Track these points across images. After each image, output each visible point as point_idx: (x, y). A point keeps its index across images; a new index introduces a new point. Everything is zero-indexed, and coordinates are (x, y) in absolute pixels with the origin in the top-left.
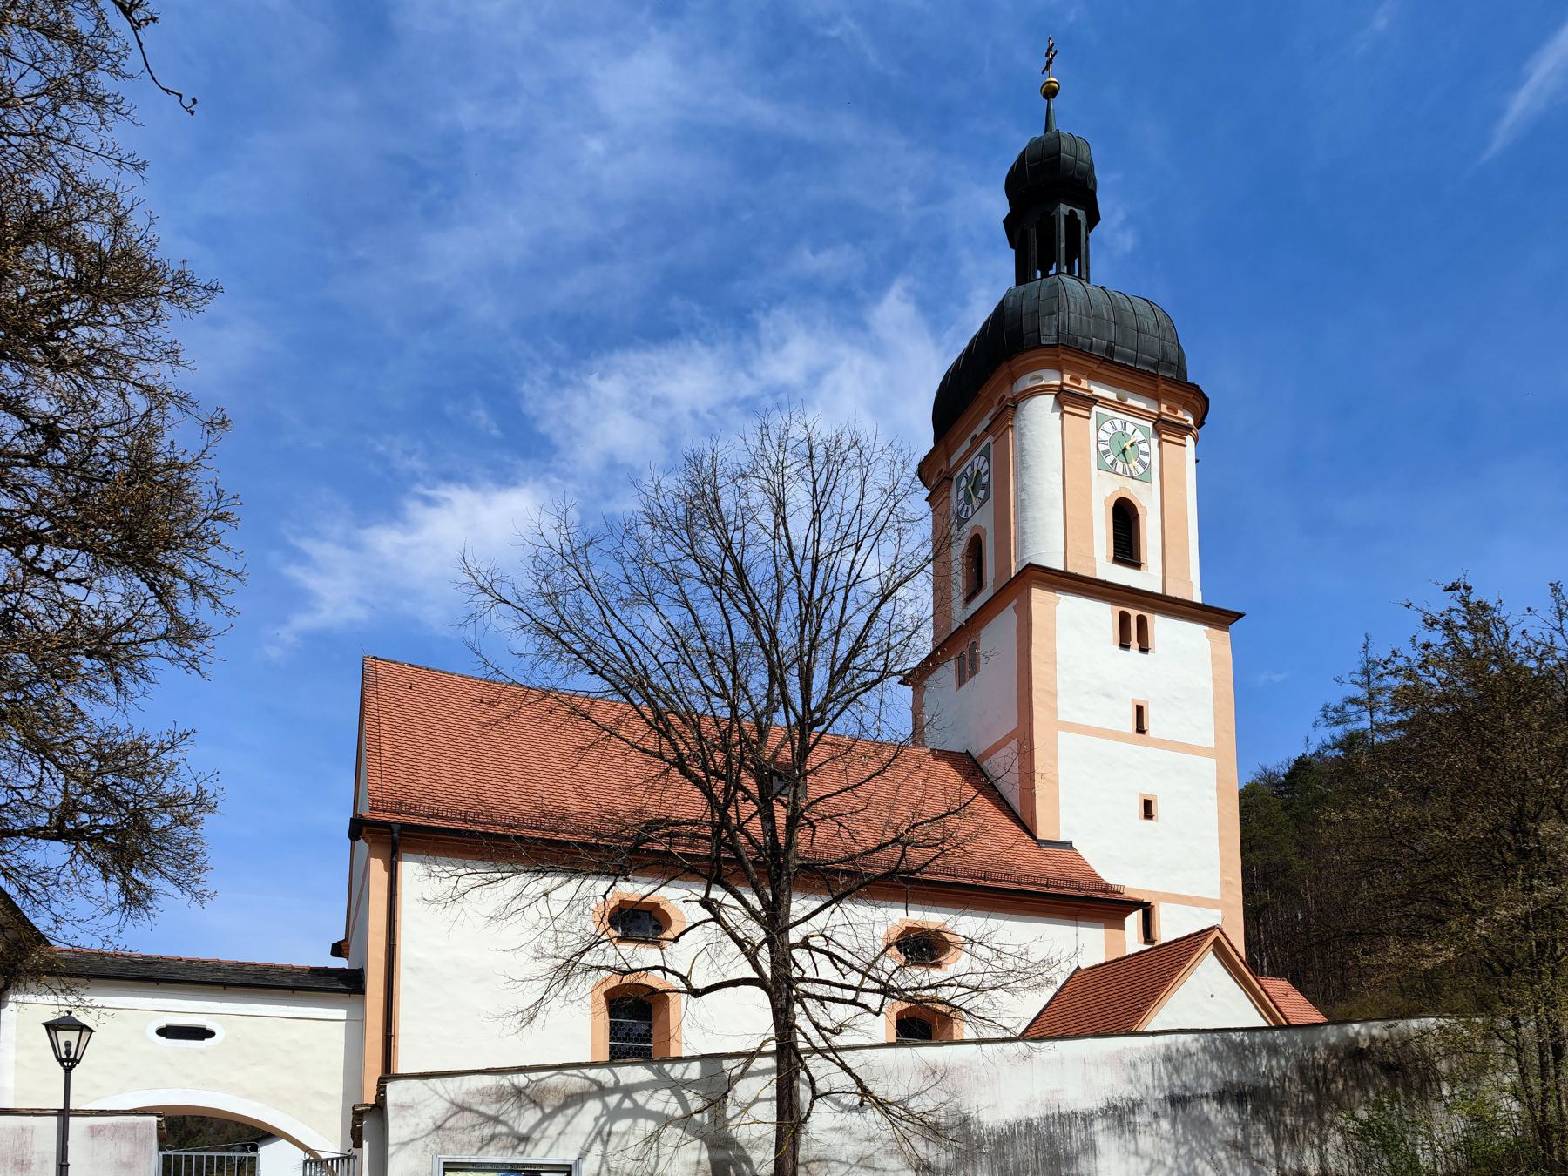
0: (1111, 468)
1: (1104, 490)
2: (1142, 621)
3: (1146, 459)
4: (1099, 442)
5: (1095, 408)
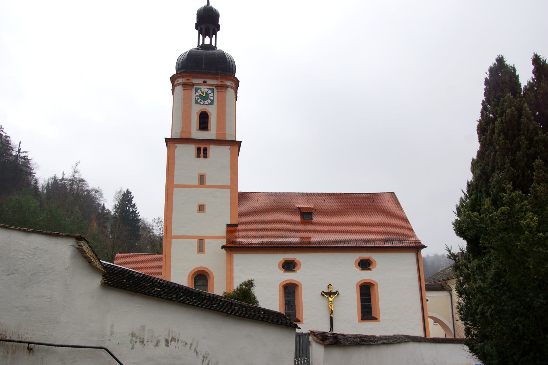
1: (196, 110)
2: (206, 150)
3: (212, 98)
5: (195, 86)
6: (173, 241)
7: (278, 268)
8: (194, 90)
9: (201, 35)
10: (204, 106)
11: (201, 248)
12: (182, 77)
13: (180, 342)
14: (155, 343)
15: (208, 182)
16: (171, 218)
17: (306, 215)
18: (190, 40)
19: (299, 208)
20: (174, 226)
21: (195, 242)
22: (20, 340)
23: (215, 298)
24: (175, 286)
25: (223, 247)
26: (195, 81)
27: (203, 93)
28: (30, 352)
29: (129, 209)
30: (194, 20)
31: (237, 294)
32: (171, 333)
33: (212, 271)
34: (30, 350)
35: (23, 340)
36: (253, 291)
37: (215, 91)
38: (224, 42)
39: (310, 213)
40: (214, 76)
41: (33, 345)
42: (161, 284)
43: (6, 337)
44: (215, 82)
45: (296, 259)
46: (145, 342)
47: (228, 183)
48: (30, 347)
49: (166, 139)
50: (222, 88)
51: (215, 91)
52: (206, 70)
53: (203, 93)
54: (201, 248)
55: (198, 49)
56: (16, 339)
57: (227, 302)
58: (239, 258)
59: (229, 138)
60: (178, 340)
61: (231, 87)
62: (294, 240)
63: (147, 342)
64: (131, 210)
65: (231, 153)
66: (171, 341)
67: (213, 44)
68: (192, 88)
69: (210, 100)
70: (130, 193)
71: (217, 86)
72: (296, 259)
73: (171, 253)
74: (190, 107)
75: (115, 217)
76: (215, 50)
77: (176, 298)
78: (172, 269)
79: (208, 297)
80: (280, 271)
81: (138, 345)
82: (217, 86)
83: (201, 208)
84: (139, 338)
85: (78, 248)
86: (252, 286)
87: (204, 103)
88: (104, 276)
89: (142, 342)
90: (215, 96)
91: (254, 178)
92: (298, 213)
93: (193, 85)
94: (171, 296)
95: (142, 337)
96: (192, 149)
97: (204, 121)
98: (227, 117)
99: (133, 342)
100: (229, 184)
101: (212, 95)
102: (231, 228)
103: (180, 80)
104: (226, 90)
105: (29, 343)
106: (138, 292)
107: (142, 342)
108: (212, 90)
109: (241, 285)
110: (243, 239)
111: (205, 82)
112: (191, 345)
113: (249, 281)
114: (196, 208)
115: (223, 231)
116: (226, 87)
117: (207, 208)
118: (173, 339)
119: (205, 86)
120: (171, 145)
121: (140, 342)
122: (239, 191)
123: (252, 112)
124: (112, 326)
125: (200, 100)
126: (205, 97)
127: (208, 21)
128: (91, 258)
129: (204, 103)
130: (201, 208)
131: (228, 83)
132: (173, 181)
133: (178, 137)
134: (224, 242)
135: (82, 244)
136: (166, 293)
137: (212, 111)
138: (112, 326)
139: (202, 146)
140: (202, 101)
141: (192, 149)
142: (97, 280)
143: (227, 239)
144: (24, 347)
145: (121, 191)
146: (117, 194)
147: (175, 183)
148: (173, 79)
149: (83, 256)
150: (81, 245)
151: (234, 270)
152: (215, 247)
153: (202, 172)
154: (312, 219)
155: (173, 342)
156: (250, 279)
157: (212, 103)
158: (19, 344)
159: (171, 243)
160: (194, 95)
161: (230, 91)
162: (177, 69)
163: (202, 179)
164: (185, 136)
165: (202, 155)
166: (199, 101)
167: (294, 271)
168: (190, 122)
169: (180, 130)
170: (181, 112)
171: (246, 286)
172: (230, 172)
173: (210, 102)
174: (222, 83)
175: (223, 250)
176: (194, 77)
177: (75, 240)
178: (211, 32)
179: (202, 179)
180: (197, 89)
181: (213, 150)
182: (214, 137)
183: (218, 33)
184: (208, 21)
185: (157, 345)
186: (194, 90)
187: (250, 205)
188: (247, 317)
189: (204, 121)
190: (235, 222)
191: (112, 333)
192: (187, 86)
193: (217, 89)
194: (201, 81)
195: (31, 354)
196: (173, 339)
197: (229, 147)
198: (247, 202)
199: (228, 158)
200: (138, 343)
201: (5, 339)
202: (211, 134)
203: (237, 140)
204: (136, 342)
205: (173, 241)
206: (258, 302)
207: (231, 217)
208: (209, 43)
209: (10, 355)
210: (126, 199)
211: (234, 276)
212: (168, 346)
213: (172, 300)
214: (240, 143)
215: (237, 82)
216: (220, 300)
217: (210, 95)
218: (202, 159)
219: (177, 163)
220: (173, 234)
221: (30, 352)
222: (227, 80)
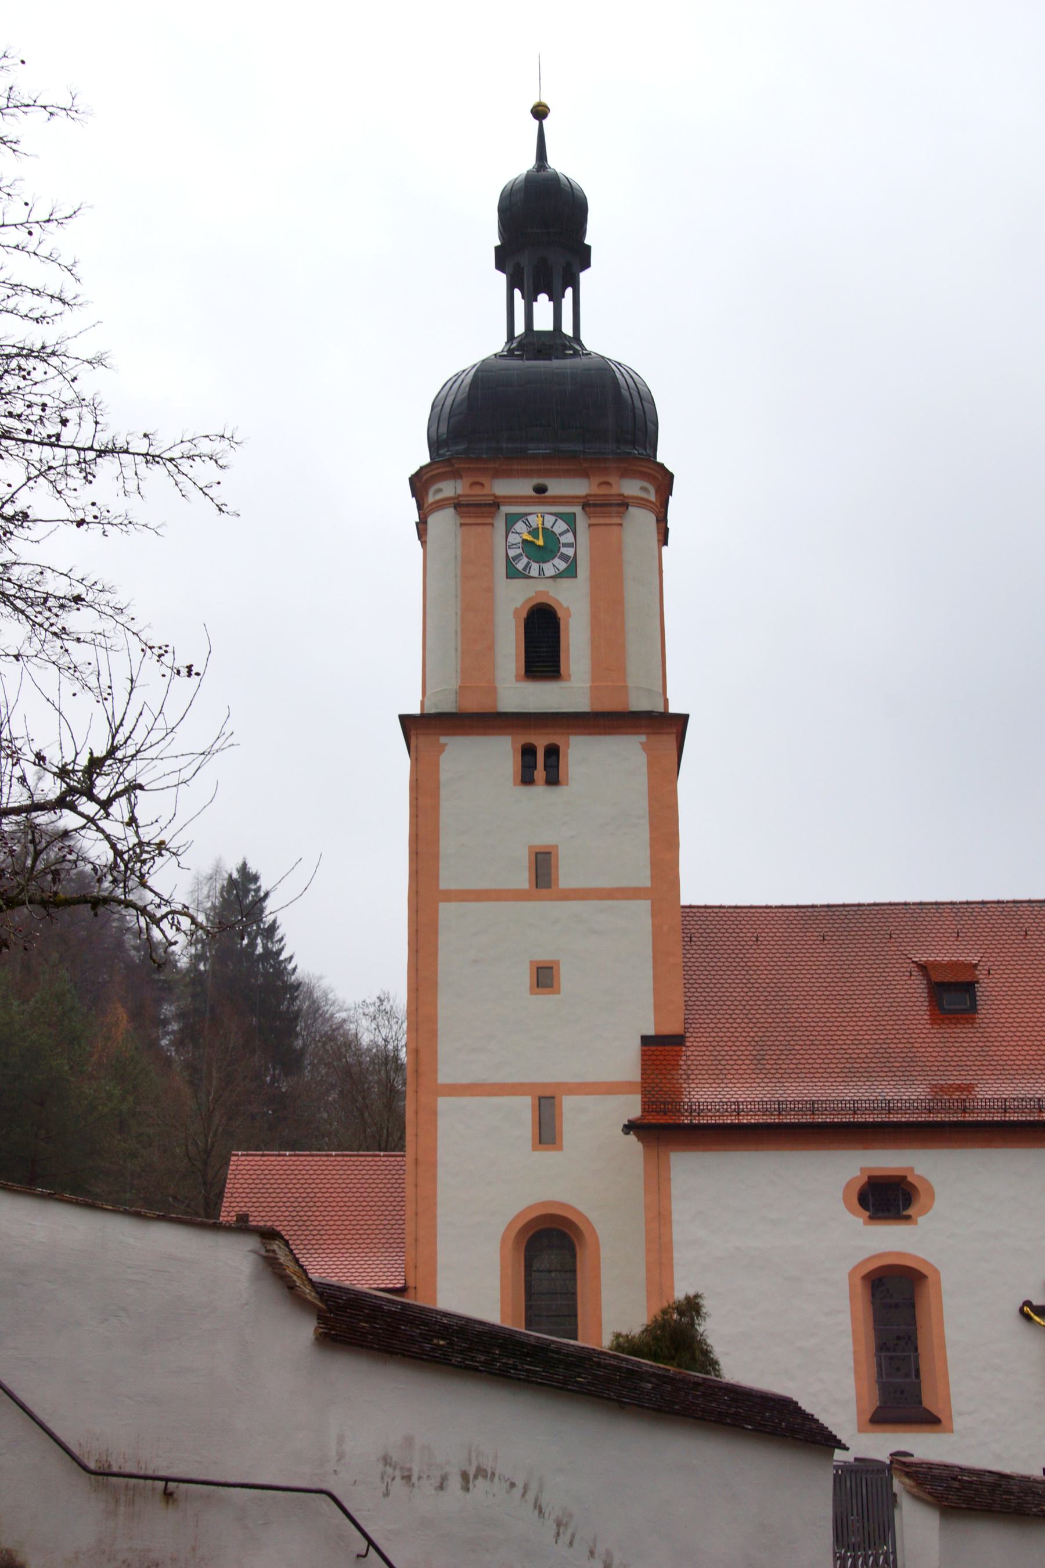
0: (524, 575)
1: (512, 600)
2: (553, 752)
3: (570, 552)
4: (509, 546)
5: (505, 509)
6: (444, 1103)
7: (842, 1206)
8: (500, 524)
9: (517, 293)
10: (542, 586)
11: (546, 1132)
12: (456, 474)
13: (496, 1479)
14: (436, 1481)
15: (567, 877)
16: (433, 1019)
17: (952, 995)
18: (474, 321)
19: (923, 968)
20: (444, 1048)
21: (524, 1106)
22: (142, 1473)
23: (587, 1359)
24: (479, 1328)
25: (630, 1127)
26: (502, 488)
27: (534, 532)
28: (167, 1503)
29: (252, 945)
30: (489, 235)
31: (656, 1338)
32: (473, 1454)
33: (592, 1216)
34: (168, 1495)
35: (150, 1473)
36: (701, 1329)
37: (582, 523)
38: (613, 317)
39: (968, 988)
40: (574, 464)
41: (175, 1484)
42: (446, 1327)
43: (110, 1466)
44: (579, 487)
45: (912, 1169)
46: (414, 1479)
47: (643, 878)
48: (169, 1489)
49: (404, 720)
50: (606, 508)
51: (582, 523)
52: (544, 439)
53: (534, 532)
54: (546, 1132)
55: (510, 354)
56: (134, 1471)
57: (618, 1369)
58: (692, 1172)
59: (639, 703)
60: (493, 1474)
61: (642, 503)
62: (907, 1094)
63: (420, 1478)
64: (260, 950)
65: (651, 764)
66: (476, 1477)
67: (567, 329)
68: (492, 515)
69: (564, 558)
70: (255, 878)
71: (588, 504)
72: (912, 1169)
73: (434, 1149)
74: (490, 590)
75: (194, 976)
76: (576, 354)
77: (486, 1363)
78: (440, 1211)
79: (567, 1355)
80: (849, 1217)
81: (398, 1487)
82: (588, 504)
83: (544, 977)
84: (402, 1468)
85: (264, 1257)
86: (698, 1313)
87: (541, 571)
88: (320, 1317)
89: (407, 1478)
90: (580, 542)
91: (752, 836)
92: (918, 986)
93: (495, 504)
94: (473, 1359)
95: (408, 1465)
96: (500, 753)
97: (542, 642)
98: (631, 622)
99: (386, 1479)
100: (647, 883)
101: (568, 538)
102: (660, 1050)
103: (449, 489)
104: (621, 515)
105: (167, 1480)
106: (397, 1354)
107: (407, 1478)
108: (570, 520)
109: (664, 1312)
110: (706, 1095)
111: (540, 490)
112: (526, 1488)
113: (688, 1298)
114: (525, 977)
115: (626, 1063)
116: (624, 504)
117: (566, 977)
118: (481, 1472)
119: (541, 505)
120: (421, 741)
121: (403, 1478)
122: (684, 901)
123: (728, 590)
124: (341, 1439)
125: (525, 560)
126: (543, 549)
127: (543, 232)
128: (295, 1278)
129: (541, 571)
130: (544, 977)
131: (631, 487)
132: (437, 877)
133: (449, 707)
134: (632, 1107)
135: (275, 1247)
136: (461, 1352)
137: (573, 601)
138: (341, 1439)
139: (541, 742)
140: (535, 566)
141: (500, 753)
142: (306, 1329)
143: (644, 1095)
144: (154, 1489)
145: (217, 871)
146: (198, 883)
147: (443, 885)
148: (419, 484)
149: (275, 1273)
150: (274, 1251)
151: (675, 1217)
152: (600, 1125)
153: (543, 839)
154: (973, 1008)
155: (480, 1479)
156: (691, 1293)
157: (571, 572)
158: (142, 1481)
159: (435, 1113)
160: (503, 542)
161: (641, 519)
162: (435, 444)
163: (543, 866)
164: (472, 706)
165: (540, 773)
166: (520, 566)
167: (908, 1218)
168: (491, 647)
169: (453, 683)
170: (456, 613)
171: (681, 1314)
172: (645, 835)
173: (562, 565)
174: (604, 491)
175: (632, 1138)
176: (497, 474)
177: (259, 1239)
178: (557, 282)
179: (543, 866)
180: (511, 520)
181: (582, 754)
182: (581, 703)
183: (585, 277)
184: (543, 232)
185: (441, 1487)
186: (500, 524)
187: (725, 952)
188: (677, 1413)
189: (542, 642)
190: (673, 1027)
191: (341, 1456)
192: (476, 511)
193: (589, 515)
194: (524, 487)
195: (170, 1506)
196: (481, 1472)
197: (643, 738)
198: (714, 944)
199: (640, 783)
200: (398, 1480)
201: (107, 1471)
202: (571, 692)
203: (672, 710)
204: (393, 1479)
205: (444, 1103)
206: (717, 1363)
207: (657, 1007)
208: (549, 326)
209: (122, 1509)
210: (240, 902)
211: (675, 1237)
212: (467, 1490)
213: (476, 1369)
214: (682, 720)
215: (664, 481)
216: (598, 1364)
217: (563, 539)
218: (540, 791)
219: (450, 809)
220: (442, 1079)
221: (167, 1503)
222: (625, 474)
